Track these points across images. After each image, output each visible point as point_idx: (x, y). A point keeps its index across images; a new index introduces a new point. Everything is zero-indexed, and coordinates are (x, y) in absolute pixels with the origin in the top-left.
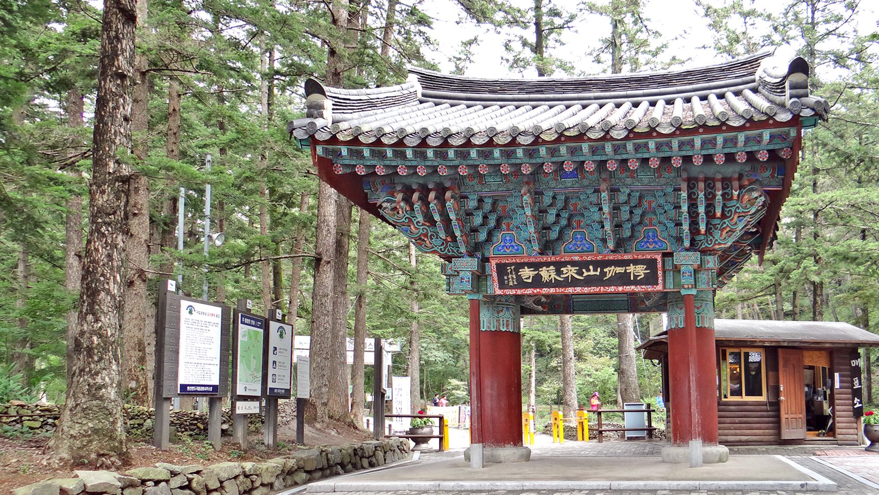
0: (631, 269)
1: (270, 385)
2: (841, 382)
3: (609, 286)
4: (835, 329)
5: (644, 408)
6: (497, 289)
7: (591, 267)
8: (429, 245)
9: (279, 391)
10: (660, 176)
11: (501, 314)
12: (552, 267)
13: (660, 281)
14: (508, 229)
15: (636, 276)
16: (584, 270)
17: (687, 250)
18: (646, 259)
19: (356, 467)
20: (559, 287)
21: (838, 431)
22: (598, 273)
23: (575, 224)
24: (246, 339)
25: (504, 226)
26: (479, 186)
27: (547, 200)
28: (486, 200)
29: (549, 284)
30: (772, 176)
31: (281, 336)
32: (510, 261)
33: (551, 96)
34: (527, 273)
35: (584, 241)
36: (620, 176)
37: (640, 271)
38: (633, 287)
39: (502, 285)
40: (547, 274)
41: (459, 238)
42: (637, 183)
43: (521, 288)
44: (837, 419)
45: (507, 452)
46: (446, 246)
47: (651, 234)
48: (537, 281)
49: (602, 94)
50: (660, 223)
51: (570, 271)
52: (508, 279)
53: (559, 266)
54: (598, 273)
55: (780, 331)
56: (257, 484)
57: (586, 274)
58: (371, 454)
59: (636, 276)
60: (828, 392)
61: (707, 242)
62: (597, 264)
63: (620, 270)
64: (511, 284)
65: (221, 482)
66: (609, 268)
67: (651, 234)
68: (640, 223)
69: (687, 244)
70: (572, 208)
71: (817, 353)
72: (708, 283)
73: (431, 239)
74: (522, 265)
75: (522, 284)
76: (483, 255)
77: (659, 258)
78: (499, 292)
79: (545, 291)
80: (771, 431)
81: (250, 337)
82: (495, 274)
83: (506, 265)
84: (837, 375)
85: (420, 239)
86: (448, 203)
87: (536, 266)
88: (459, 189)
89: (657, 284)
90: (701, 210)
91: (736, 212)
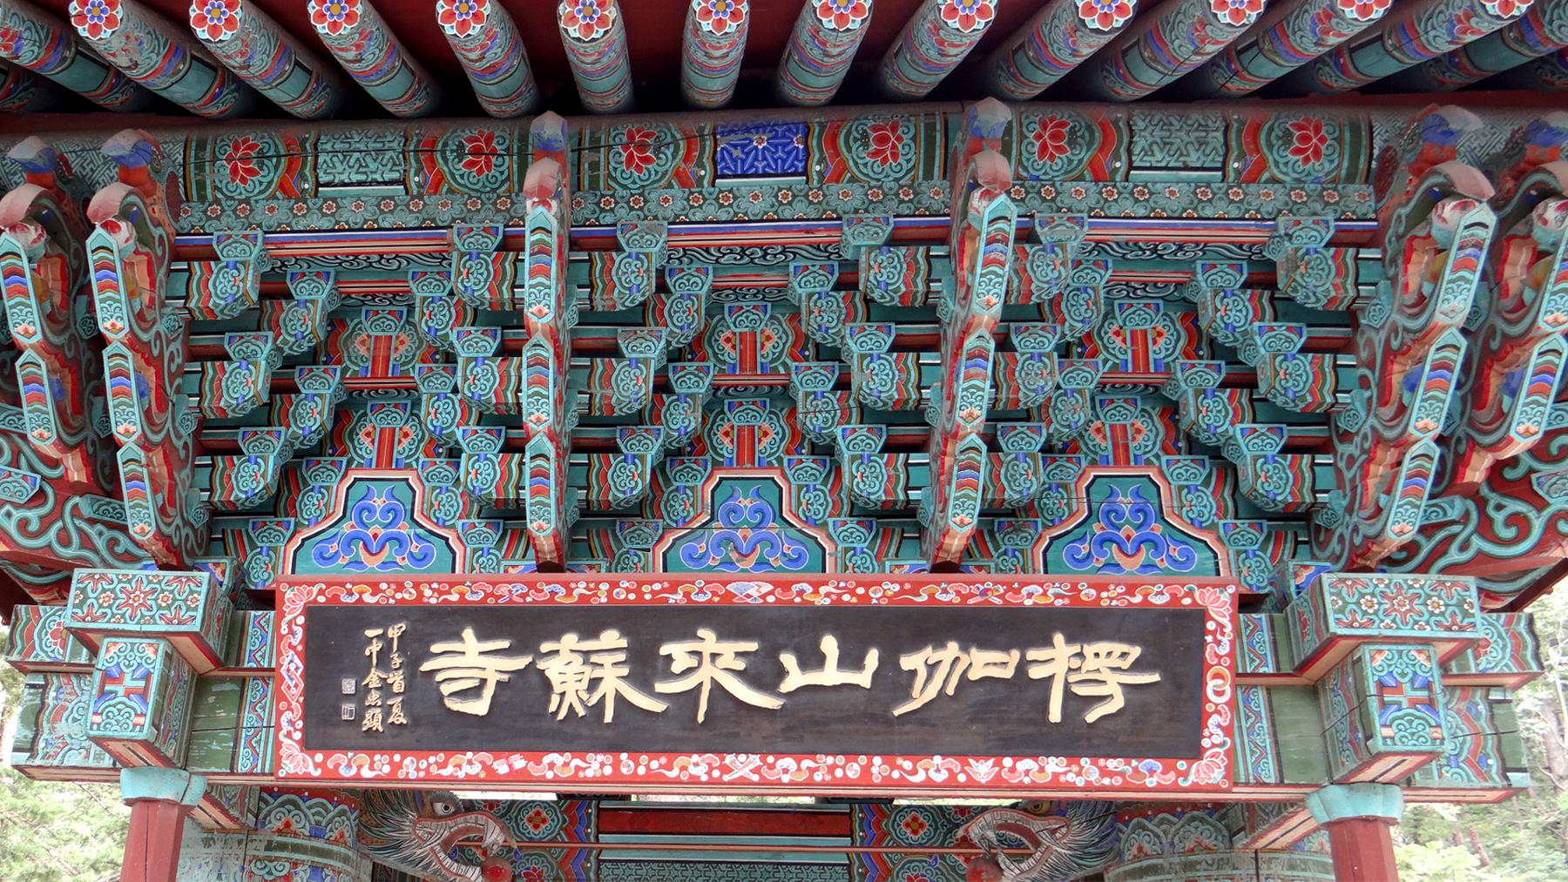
0: (1055, 661)
3: (919, 751)
6: (290, 747)
7: (830, 645)
10: (1252, 176)
12: (611, 638)
13: (1213, 734)
14: (385, 458)
16: (788, 660)
20: (635, 750)
22: (864, 679)
23: (727, 447)
25: (366, 447)
26: (282, 204)
27: (629, 280)
28: (301, 290)
29: (584, 732)
34: (470, 665)
35: (774, 528)
37: (1106, 673)
38: (1054, 765)
39: (324, 727)
40: (578, 672)
41: (129, 449)
42: (1128, 207)
43: (419, 748)
46: (57, 513)
47: (1125, 502)
51: (709, 663)
53: (648, 630)
54: (864, 679)
57: (796, 679)
61: (1485, 528)
62: (861, 627)
63: (987, 663)
64: (373, 720)
66: (928, 654)
67: (1125, 502)
70: (730, 355)
72: (1477, 762)
74: (444, 621)
75: (435, 725)
76: (240, 574)
77: (1219, 606)
78: (298, 764)
82: (292, 666)
83: (362, 616)
86: (98, 236)
87: (523, 627)
88: (175, 210)
89: (1196, 753)
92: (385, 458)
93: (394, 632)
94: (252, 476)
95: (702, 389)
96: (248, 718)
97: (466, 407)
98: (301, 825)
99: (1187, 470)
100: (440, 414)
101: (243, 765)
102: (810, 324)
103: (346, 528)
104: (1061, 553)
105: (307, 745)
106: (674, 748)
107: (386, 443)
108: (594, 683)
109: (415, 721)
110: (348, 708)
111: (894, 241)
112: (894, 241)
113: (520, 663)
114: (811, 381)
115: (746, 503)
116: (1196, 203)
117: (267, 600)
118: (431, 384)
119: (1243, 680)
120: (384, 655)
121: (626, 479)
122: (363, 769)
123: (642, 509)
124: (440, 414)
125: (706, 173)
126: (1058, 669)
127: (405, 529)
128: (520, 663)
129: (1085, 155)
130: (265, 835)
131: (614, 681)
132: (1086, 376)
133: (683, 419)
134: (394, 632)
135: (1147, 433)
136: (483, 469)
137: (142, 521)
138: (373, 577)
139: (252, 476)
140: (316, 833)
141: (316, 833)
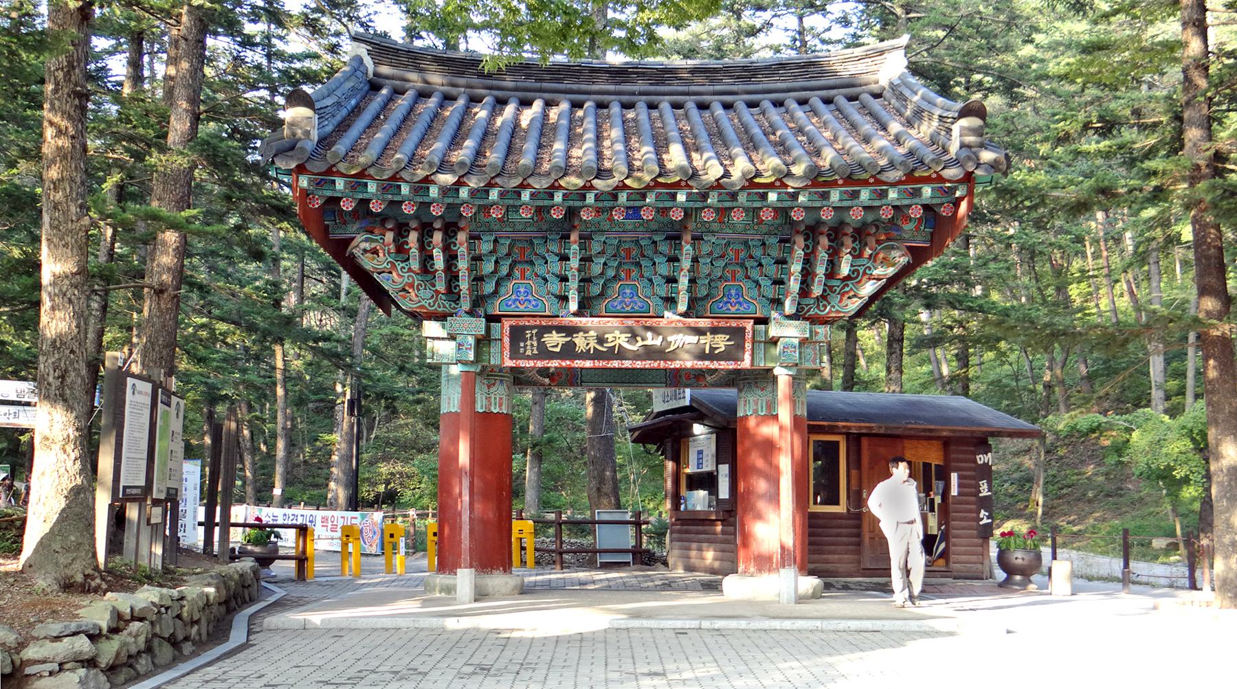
2: (960, 486)
4: (954, 409)
5: (628, 517)
8: (415, 299)
11: (493, 389)
14: (523, 277)
17: (789, 317)
18: (730, 327)
20: (599, 360)
21: (953, 557)
23: (623, 275)
25: (517, 273)
27: (596, 247)
28: (502, 241)
29: (585, 355)
32: (532, 322)
33: (575, 87)
34: (554, 340)
35: (636, 298)
39: (515, 354)
43: (542, 359)
44: (953, 540)
45: (498, 581)
47: (733, 292)
48: (568, 351)
49: (652, 88)
50: (536, 275)
52: (525, 346)
55: (868, 410)
60: (938, 500)
61: (818, 307)
64: (529, 353)
67: (733, 292)
68: (509, 275)
69: (789, 307)
71: (925, 443)
74: (548, 329)
78: (509, 363)
79: (578, 363)
80: (851, 557)
82: (507, 340)
83: (525, 328)
84: (954, 477)
90: (821, 270)
91: (865, 273)
93: (534, 332)
99: (750, 284)
101: (492, 362)
105: (511, 358)
109: (540, 353)
110: (522, 350)
111: (666, 239)
112: (666, 239)
115: (628, 291)
121: (595, 290)
122: (523, 363)
123: (602, 295)
126: (708, 341)
127: (530, 297)
131: (593, 344)
132: (721, 263)
133: (611, 273)
134: (534, 332)
135: (740, 274)
136: (555, 286)
139: (489, 288)
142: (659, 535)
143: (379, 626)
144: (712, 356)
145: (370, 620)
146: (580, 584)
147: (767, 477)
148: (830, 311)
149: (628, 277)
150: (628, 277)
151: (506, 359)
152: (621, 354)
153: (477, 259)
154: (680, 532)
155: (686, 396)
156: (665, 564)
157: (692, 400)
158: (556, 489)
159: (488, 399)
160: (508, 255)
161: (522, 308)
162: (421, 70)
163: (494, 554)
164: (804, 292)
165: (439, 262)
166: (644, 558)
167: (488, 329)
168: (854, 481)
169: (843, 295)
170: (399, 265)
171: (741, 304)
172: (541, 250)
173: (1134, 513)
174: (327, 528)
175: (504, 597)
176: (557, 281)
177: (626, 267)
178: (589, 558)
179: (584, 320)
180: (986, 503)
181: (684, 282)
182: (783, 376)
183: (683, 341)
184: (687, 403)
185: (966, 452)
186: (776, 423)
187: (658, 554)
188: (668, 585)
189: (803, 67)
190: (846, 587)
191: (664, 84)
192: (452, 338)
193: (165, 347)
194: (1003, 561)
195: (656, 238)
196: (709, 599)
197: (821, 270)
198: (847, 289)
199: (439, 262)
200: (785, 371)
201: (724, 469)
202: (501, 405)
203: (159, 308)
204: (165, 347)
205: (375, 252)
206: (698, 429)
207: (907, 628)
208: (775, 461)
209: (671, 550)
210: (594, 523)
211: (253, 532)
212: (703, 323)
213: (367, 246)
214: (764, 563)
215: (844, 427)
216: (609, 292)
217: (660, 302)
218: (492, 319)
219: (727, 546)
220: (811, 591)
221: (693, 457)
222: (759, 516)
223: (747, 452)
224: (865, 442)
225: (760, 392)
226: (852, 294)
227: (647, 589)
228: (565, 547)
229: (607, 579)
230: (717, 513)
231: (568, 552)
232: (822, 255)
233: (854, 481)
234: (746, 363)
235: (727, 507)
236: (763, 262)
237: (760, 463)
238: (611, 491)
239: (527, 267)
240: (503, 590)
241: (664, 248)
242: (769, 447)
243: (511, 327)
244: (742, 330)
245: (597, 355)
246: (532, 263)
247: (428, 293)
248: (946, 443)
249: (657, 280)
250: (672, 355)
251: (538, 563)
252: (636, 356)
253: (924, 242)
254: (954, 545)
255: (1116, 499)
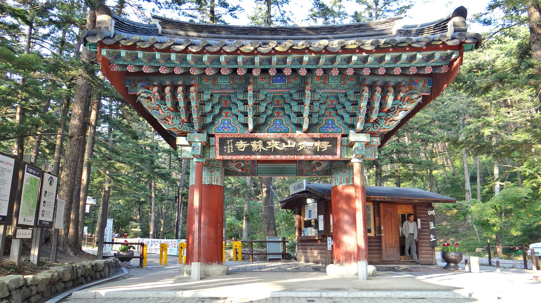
1: (41, 218)
2: (421, 225)
5: (280, 240)
6: (218, 155)
8: (171, 124)
9: (46, 223)
10: (344, 84)
11: (213, 173)
14: (227, 116)
15: (321, 149)
18: (330, 138)
19: (94, 279)
20: (264, 155)
23: (276, 114)
24: (28, 184)
25: (224, 114)
27: (262, 97)
28: (215, 96)
30: (424, 86)
31: (51, 184)
33: (253, 36)
34: (241, 145)
35: (282, 126)
36: (316, 82)
38: (318, 156)
39: (222, 153)
45: (215, 268)
47: (330, 122)
48: (249, 151)
52: (227, 148)
56: (34, 293)
58: (101, 269)
59: (321, 149)
61: (373, 127)
64: (229, 152)
65: (10, 291)
67: (330, 122)
73: (173, 120)
74: (238, 139)
75: (237, 152)
77: (339, 137)
78: (219, 157)
79: (253, 157)
81: (31, 183)
82: (217, 145)
85: (165, 119)
87: (249, 140)
91: (398, 108)
92: (227, 116)
94: (209, 120)
95: (272, 108)
96: (211, 151)
97: (239, 111)
98: (215, 164)
99: (338, 118)
100: (234, 111)
101: (211, 157)
102: (286, 101)
103: (222, 126)
104: (321, 129)
105: (220, 155)
106: (269, 155)
107: (227, 114)
108: (258, 147)
113: (248, 144)
114: (286, 107)
115: (278, 122)
116: (337, 87)
117: (213, 136)
118: (233, 107)
119: (342, 145)
120: (230, 144)
121: (262, 120)
122: (226, 157)
124: (234, 111)
125: (271, 82)
126: (319, 145)
127: (230, 126)
128: (248, 144)
129: (322, 81)
130: (210, 165)
131: (261, 147)
132: (324, 107)
133: (269, 112)
135: (333, 113)
136: (242, 119)
137: (196, 127)
138: (227, 134)
139: (209, 120)
140: (217, 165)
141: (217, 165)
142: (292, 248)
143: (137, 297)
144: (321, 153)
145: (132, 293)
146: (259, 268)
147: (348, 213)
148: (380, 129)
149: (278, 115)
150: (278, 115)
151: (218, 155)
152: (276, 152)
153: (203, 104)
154: (302, 245)
155: (304, 183)
156: (296, 259)
157: (306, 188)
158: (255, 234)
159: (211, 178)
160: (219, 103)
161: (226, 131)
162: (185, 30)
163: (214, 255)
164: (367, 119)
165: (182, 104)
166: (286, 257)
167: (208, 140)
168: (377, 223)
169: (387, 120)
170: (163, 107)
171: (334, 128)
172: (234, 100)
173: (464, 239)
174: (153, 246)
175: (218, 277)
176: (242, 116)
177: (277, 111)
178: (264, 257)
179: (256, 134)
180: (433, 232)
181: (306, 114)
182: (356, 163)
183: (307, 144)
184: (305, 189)
185: (423, 210)
186: (352, 187)
187: (292, 255)
188: (298, 270)
189: (357, 27)
190: (393, 269)
191: (294, 35)
192: (190, 145)
193: (72, 161)
194: (445, 257)
195: (292, 92)
196: (321, 277)
197: (377, 105)
198: (389, 117)
199: (182, 104)
200: (358, 160)
201: (321, 217)
202: (217, 181)
203: (70, 145)
204: (72, 161)
205: (149, 98)
206: (309, 201)
207: (440, 296)
208: (353, 206)
209: (298, 253)
210: (266, 242)
211: (123, 247)
212: (316, 135)
213: (145, 95)
214: (349, 257)
215: (373, 198)
216: (269, 123)
217: (294, 127)
218: (210, 136)
219: (323, 251)
220: (371, 273)
221: (307, 213)
222: (345, 233)
223: (337, 202)
224: (381, 205)
225: (342, 174)
226: (391, 119)
227: (289, 271)
228: (254, 252)
229: (272, 267)
230: (318, 236)
231: (254, 254)
232: (378, 95)
233: (377, 223)
234: (337, 157)
235: (322, 234)
236: (346, 105)
237: (345, 206)
238: (272, 228)
239: (228, 111)
240: (218, 273)
241: (296, 97)
242: (349, 199)
243: (219, 138)
244: (335, 139)
245: (263, 153)
246: (231, 109)
247: (178, 122)
248: (415, 206)
249: (293, 104)
250: (301, 153)
251: (243, 259)
252: (284, 152)
253: (427, 92)
254: (421, 250)
255: (456, 234)
